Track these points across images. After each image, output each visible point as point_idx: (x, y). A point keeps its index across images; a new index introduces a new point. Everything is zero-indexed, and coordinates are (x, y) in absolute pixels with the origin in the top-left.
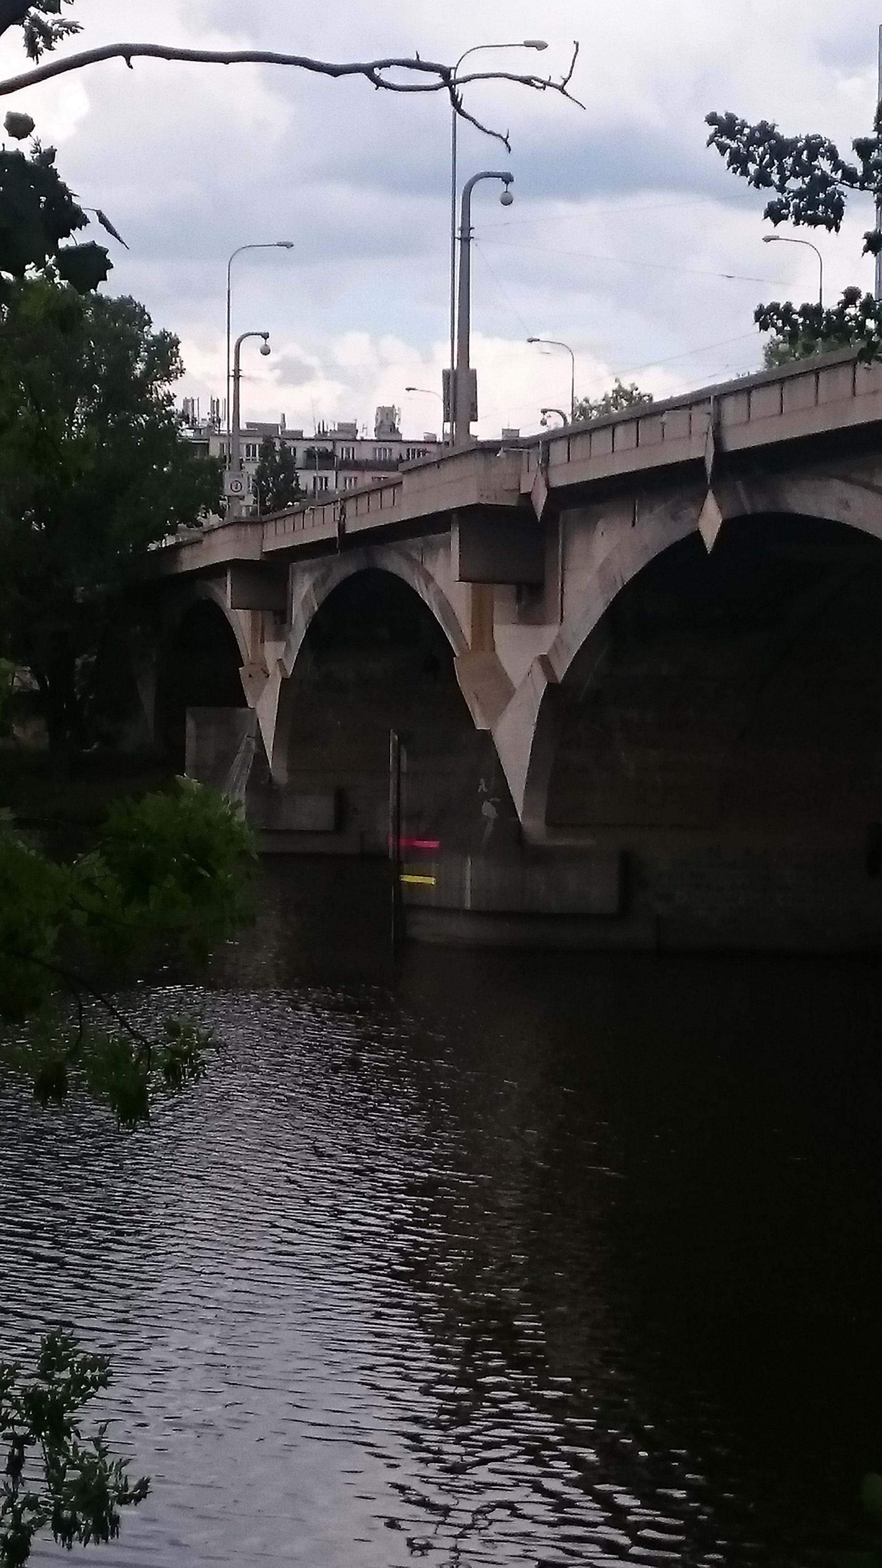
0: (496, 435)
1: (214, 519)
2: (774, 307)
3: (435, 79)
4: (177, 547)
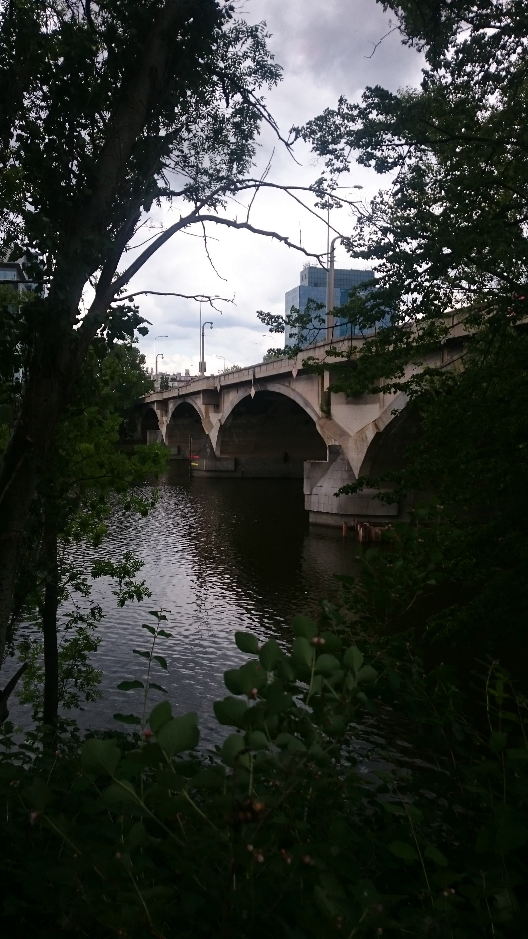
0: (210, 375)
1: (152, 392)
2: (271, 349)
3: (207, 299)
4: (144, 398)
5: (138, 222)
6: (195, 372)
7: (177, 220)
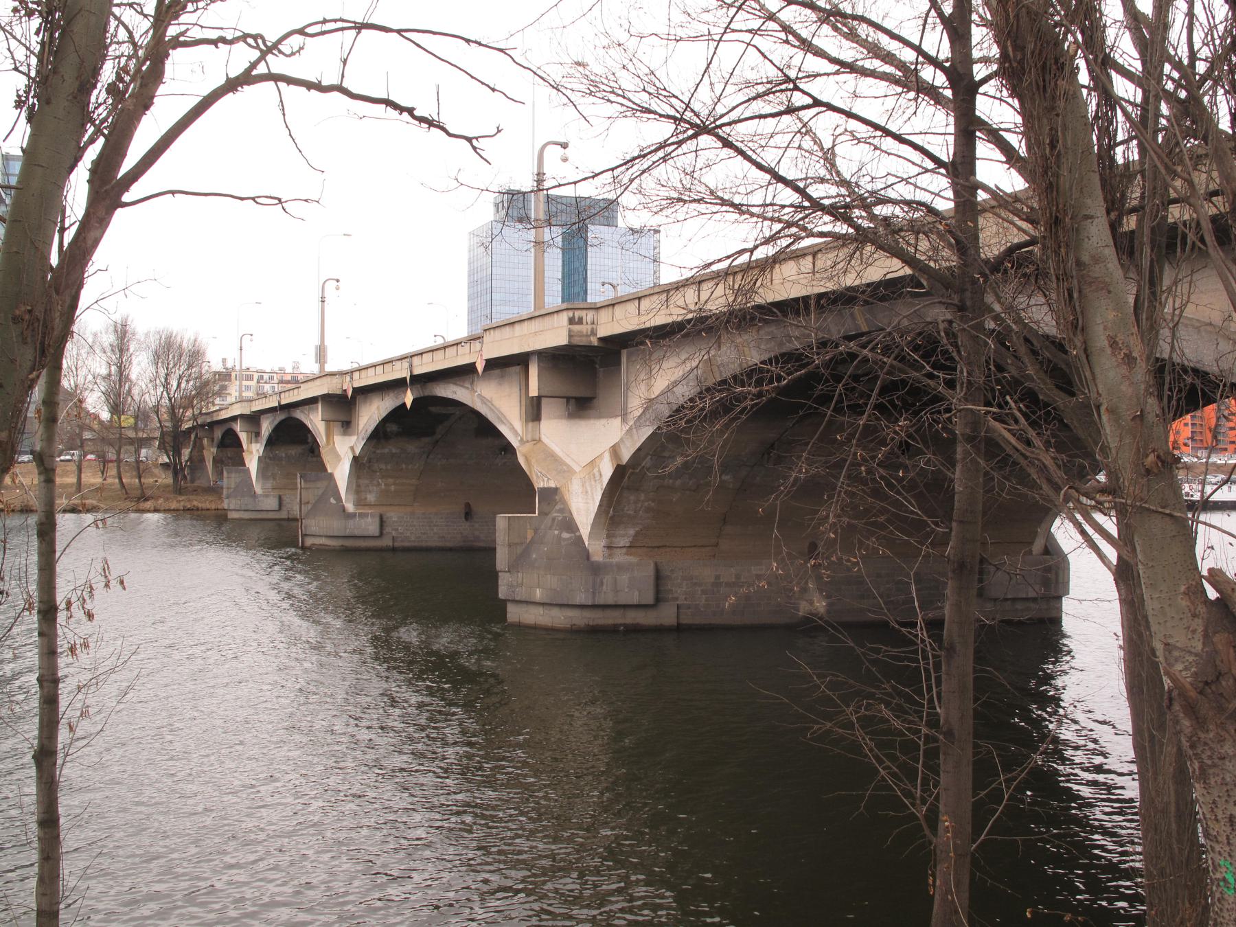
5: (162, 85)
6: (310, 367)
7: (221, 81)
